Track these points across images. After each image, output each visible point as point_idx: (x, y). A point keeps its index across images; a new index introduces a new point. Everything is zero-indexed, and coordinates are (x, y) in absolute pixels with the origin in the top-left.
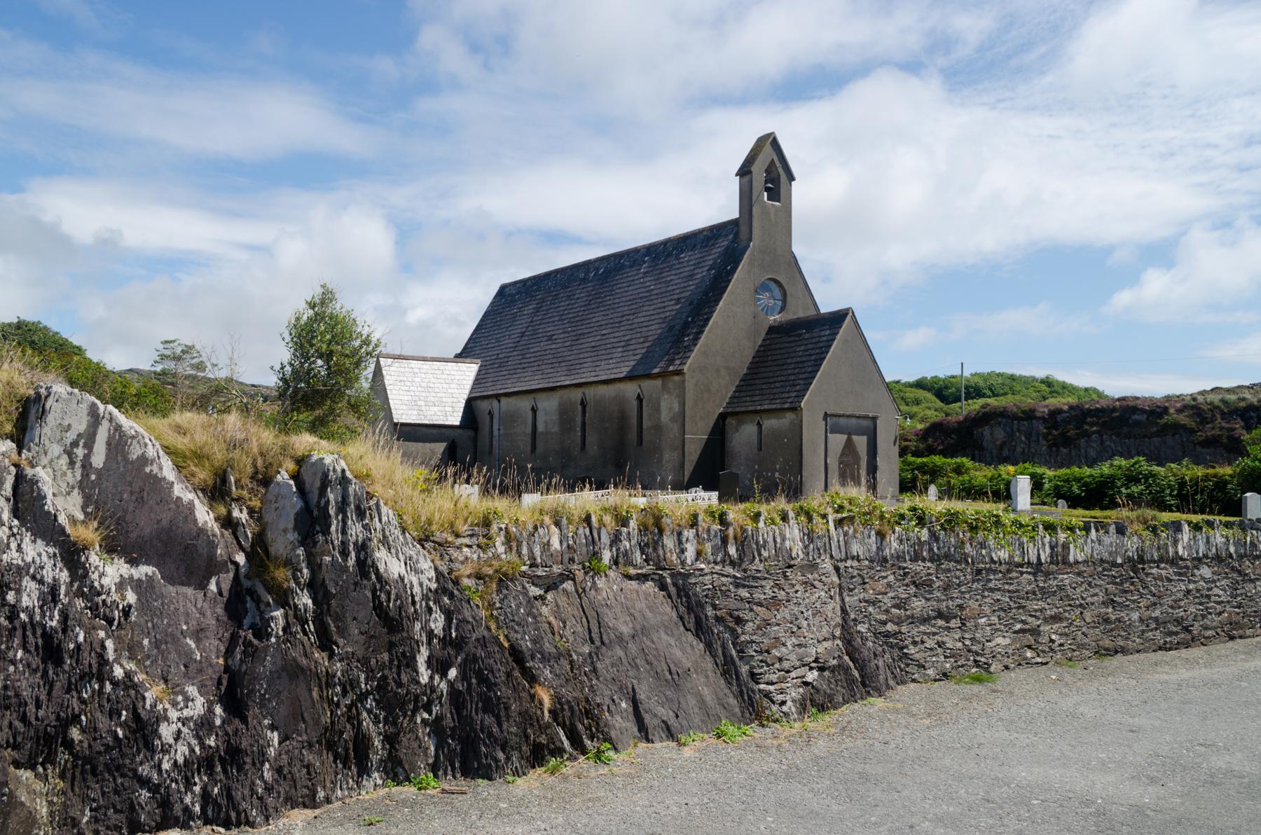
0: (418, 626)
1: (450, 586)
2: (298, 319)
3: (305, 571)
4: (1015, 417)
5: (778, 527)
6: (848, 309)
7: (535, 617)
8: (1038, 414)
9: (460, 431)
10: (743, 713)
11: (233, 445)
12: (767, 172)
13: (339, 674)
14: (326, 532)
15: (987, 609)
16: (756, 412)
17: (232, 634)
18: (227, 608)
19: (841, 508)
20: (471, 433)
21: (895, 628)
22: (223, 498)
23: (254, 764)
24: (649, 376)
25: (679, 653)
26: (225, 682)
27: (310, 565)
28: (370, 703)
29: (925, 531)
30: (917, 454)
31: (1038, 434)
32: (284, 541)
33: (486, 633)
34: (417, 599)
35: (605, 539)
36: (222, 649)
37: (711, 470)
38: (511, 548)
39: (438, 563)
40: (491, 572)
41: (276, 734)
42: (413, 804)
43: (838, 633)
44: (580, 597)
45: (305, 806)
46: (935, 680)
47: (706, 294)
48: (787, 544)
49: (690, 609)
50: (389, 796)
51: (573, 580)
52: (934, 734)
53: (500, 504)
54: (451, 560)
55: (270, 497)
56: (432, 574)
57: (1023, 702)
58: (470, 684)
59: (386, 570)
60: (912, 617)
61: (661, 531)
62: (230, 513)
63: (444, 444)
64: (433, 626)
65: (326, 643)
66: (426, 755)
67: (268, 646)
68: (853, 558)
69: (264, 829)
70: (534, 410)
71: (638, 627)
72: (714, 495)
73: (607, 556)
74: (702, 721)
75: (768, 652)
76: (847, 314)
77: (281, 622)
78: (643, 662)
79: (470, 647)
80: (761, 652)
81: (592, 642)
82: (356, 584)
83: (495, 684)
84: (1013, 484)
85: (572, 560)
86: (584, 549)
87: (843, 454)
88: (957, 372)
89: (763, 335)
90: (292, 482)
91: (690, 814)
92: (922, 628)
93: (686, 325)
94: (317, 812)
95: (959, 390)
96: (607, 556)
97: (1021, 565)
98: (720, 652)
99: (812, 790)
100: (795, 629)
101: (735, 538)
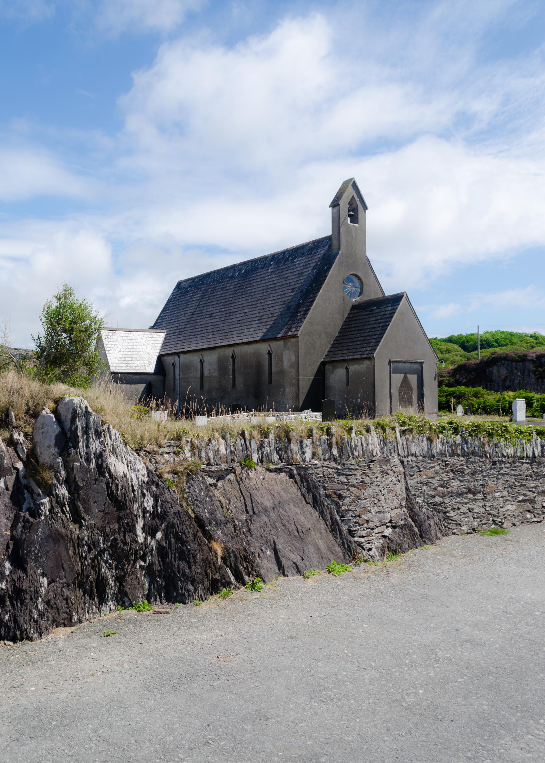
0: (136, 506)
1: (156, 479)
2: (49, 308)
3: (63, 472)
4: (513, 360)
5: (364, 437)
6: (403, 293)
7: (210, 498)
8: (529, 358)
9: (154, 377)
10: (344, 556)
11: (12, 393)
12: (349, 206)
13: (86, 538)
14: (76, 447)
15: (500, 487)
16: (344, 361)
17: (15, 515)
18: (12, 498)
19: (404, 423)
20: (160, 378)
21: (441, 500)
22: (7, 427)
23: (31, 599)
24: (275, 339)
25: (302, 519)
26: (11, 547)
27: (66, 469)
28: (106, 556)
29: (459, 437)
30: (449, 385)
31: (529, 371)
32: (48, 453)
33: (180, 509)
34: (135, 488)
35: (254, 446)
36: (9, 525)
37: (316, 398)
38: (194, 454)
39: (148, 464)
40: (182, 470)
41: (45, 579)
42: (135, 622)
43: (404, 503)
44: (239, 484)
45: (65, 625)
46: (468, 533)
47: (311, 285)
48: (370, 447)
49: (309, 490)
50: (119, 616)
51: (235, 473)
52: (468, 568)
53: (183, 424)
54: (156, 463)
55: (38, 425)
56: (145, 472)
57: (526, 547)
58: (170, 542)
59: (115, 470)
60: (452, 492)
61: (289, 440)
62: (12, 436)
63: (144, 385)
64: (146, 505)
65: (77, 518)
66: (143, 589)
67: (39, 522)
68: (412, 455)
69: (39, 641)
70: (202, 362)
71: (276, 502)
72: (319, 415)
73: (255, 457)
74: (319, 562)
75: (359, 516)
76: (403, 296)
77: (48, 506)
78: (280, 525)
79: (170, 518)
80: (355, 517)
81: (247, 512)
82: (96, 480)
83: (187, 542)
84: (513, 404)
85: (233, 460)
86: (241, 453)
87: (401, 387)
88: (475, 331)
89: (348, 311)
90: (52, 415)
91: (313, 623)
92: (458, 500)
93: (299, 306)
94: (73, 629)
95: (476, 343)
96: (255, 457)
97: (522, 458)
98: (329, 517)
99: (391, 606)
100: (376, 502)
101: (337, 444)
